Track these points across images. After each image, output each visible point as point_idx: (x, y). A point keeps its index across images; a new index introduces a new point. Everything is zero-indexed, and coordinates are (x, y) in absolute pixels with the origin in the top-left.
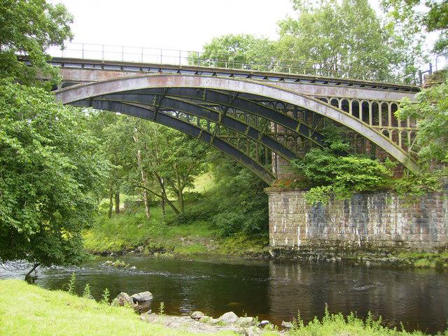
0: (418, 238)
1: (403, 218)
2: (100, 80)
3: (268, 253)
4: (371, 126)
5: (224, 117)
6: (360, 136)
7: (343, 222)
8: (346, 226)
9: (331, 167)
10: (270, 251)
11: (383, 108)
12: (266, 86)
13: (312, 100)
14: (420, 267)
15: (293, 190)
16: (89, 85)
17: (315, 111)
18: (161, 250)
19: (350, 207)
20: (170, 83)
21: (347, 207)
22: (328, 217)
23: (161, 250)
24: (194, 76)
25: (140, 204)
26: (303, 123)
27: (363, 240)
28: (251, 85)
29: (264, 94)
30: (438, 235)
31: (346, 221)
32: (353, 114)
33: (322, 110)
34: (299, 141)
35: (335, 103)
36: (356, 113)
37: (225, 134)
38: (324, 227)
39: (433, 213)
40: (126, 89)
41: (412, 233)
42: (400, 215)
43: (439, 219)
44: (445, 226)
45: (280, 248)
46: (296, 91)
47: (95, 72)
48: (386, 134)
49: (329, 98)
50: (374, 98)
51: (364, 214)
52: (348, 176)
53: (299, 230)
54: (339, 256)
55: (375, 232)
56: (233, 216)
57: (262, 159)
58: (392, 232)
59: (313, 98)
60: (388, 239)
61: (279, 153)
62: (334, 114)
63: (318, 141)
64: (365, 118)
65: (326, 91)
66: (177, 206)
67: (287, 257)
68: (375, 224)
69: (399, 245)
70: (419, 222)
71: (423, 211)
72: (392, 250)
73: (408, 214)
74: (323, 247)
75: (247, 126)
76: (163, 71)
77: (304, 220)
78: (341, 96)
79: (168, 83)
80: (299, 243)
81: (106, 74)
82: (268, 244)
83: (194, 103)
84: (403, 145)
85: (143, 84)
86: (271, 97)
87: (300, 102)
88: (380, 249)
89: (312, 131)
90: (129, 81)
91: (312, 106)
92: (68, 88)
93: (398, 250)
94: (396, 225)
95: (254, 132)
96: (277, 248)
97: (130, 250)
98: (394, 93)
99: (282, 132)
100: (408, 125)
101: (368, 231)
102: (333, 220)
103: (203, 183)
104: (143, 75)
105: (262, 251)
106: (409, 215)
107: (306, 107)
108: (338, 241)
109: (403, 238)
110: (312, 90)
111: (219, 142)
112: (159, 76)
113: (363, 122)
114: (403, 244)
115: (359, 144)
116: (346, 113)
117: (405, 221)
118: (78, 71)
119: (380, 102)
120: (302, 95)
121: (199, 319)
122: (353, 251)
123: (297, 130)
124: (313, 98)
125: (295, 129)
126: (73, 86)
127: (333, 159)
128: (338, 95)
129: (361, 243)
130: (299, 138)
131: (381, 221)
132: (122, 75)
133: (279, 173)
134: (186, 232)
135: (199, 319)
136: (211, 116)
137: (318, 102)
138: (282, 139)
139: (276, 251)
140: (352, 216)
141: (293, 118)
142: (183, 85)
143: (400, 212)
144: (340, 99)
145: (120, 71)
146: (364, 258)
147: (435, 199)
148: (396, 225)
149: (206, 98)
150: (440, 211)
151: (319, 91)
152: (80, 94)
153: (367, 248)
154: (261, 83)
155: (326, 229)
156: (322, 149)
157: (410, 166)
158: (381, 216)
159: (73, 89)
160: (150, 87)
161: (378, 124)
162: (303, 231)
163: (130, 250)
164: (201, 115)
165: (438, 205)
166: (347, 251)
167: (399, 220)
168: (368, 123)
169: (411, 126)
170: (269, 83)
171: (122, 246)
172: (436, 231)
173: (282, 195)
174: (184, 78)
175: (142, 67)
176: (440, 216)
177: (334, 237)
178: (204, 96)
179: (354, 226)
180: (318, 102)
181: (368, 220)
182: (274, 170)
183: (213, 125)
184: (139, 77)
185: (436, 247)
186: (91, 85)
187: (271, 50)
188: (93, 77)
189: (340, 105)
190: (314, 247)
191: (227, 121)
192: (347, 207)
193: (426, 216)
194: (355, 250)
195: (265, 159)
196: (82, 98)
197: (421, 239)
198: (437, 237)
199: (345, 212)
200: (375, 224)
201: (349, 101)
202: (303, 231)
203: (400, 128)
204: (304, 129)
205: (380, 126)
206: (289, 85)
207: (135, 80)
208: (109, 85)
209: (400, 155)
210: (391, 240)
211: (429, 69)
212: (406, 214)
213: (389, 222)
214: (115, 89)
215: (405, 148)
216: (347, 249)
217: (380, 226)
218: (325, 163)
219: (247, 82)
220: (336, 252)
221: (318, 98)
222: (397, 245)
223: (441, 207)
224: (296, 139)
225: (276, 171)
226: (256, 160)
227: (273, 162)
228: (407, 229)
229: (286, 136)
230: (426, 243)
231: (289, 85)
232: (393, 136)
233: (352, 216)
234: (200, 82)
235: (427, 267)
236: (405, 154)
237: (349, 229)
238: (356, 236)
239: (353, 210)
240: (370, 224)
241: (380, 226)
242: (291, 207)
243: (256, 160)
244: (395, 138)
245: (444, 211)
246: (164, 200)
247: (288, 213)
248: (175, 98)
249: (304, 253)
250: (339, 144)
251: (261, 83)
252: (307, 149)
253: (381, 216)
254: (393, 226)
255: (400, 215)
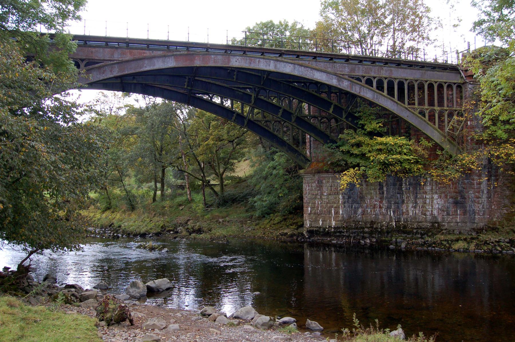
0: (456, 220)
1: (439, 200)
2: (124, 59)
3: (302, 234)
4: (406, 106)
5: (257, 99)
6: (395, 116)
7: (377, 203)
8: (380, 207)
9: (365, 149)
10: (304, 233)
11: (419, 88)
12: (298, 65)
13: (346, 79)
14: (458, 251)
15: (327, 172)
16: (113, 64)
17: (349, 90)
18: (199, 231)
19: (385, 189)
20: (198, 63)
21: (381, 188)
22: (362, 198)
23: (199, 231)
24: (222, 55)
25: (182, 187)
26: (337, 104)
27: (398, 221)
28: (283, 64)
29: (296, 73)
30: (476, 217)
31: (381, 202)
32: (388, 94)
33: (356, 90)
34: (333, 123)
35: (369, 82)
36: (391, 92)
37: (257, 114)
38: (358, 208)
39: (471, 194)
40: (152, 68)
41: (448, 214)
42: (436, 196)
43: (477, 200)
44: (483, 208)
45: (315, 229)
46: (329, 70)
47: (119, 51)
48: (422, 113)
49: (364, 77)
50: (410, 77)
51: (399, 195)
52: (382, 157)
53: (333, 211)
54: (373, 237)
55: (411, 214)
56: (268, 199)
57: (296, 141)
58: (428, 213)
59: (347, 77)
60: (423, 220)
61: (313, 135)
62: (368, 94)
63: (352, 122)
64: (401, 98)
65: (360, 71)
66: (217, 189)
67: (320, 239)
68: (411, 205)
69: (436, 227)
70: (456, 203)
71: (460, 192)
72: (427, 232)
73: (443, 195)
74: (357, 228)
75: (280, 108)
76: (191, 49)
77: (339, 202)
78: (375, 75)
79: (196, 61)
80: (333, 223)
81: (131, 53)
82: (302, 226)
83: (226, 85)
84: (439, 125)
85: (171, 63)
86: (302, 76)
87: (334, 82)
88: (415, 231)
89: (345, 112)
90: (155, 60)
91: (345, 85)
92: (91, 67)
93: (434, 231)
94: (432, 206)
95: (287, 114)
96: (312, 229)
97: (169, 231)
98: (432, 72)
99: (316, 114)
100: (445, 105)
101: (403, 213)
102: (368, 201)
103: (243, 169)
104: (170, 54)
105: (296, 232)
106: (446, 196)
107: (339, 87)
108: (372, 223)
109: (440, 220)
110: (346, 69)
111: (252, 125)
112: (186, 55)
113: (399, 102)
114: (438, 225)
115: (396, 125)
116: (381, 92)
117: (441, 202)
118: (101, 50)
119: (416, 81)
120: (335, 74)
121: (209, 315)
122: (388, 233)
123: (331, 111)
124: (347, 77)
125: (329, 110)
126: (97, 65)
127: (367, 139)
128: (373, 74)
129: (396, 224)
130: (333, 121)
131: (416, 203)
132: (148, 53)
133: (313, 155)
134: (225, 214)
135: (209, 315)
136: (245, 99)
137: (351, 81)
138: (316, 121)
139: (311, 232)
140: (387, 198)
141: (326, 98)
142: (211, 64)
143: (436, 193)
144: (375, 78)
145: (145, 49)
146: (398, 240)
147: (473, 180)
148: (432, 206)
149: (237, 79)
150: (479, 192)
151: (353, 70)
152: (103, 73)
153: (402, 229)
154: (293, 62)
155: (360, 210)
156: (355, 131)
157: (447, 147)
158: (416, 197)
159: (97, 68)
160: (177, 66)
161: (414, 104)
162: (337, 213)
163: (169, 231)
164: (234, 97)
165: (476, 186)
166: (381, 232)
167: (435, 201)
168: (404, 103)
169: (448, 106)
170: (301, 62)
171: (162, 227)
172: (474, 212)
173: (317, 177)
174: (213, 56)
175: (167, 47)
176: (478, 198)
177: (369, 219)
178: (235, 77)
179: (388, 208)
180: (351, 81)
181: (403, 202)
182: (308, 153)
183: (247, 109)
184: (165, 56)
185: (474, 229)
186: (115, 64)
187: (303, 34)
188: (117, 56)
189: (375, 84)
190: (348, 228)
191: (259, 103)
192: (381, 188)
193: (463, 197)
194: (390, 231)
195: (300, 142)
196: (106, 77)
197: (458, 220)
198: (475, 218)
199: (380, 194)
200: (411, 205)
201: (384, 80)
202: (337, 213)
203: (437, 108)
204: (338, 110)
205: (416, 106)
206: (322, 64)
207: (160, 60)
208: (133, 64)
209: (436, 136)
210: (426, 221)
211: (467, 48)
212: (443, 195)
213: (425, 203)
214: (141, 68)
215: (441, 127)
216: (382, 230)
217: (415, 207)
218: (358, 145)
219: (278, 61)
220: (371, 233)
221: (353, 78)
222: (433, 226)
223: (480, 188)
224: (329, 121)
225: (310, 153)
226: (290, 142)
227: (308, 144)
228: (443, 211)
229: (320, 119)
230: (463, 224)
231: (322, 64)
232: (429, 116)
233: (387, 198)
234: (229, 61)
235: (466, 251)
236: (442, 135)
237: (383, 210)
238: (391, 217)
239: (387, 191)
240: (405, 205)
241: (415, 207)
242: (325, 189)
243: (290, 142)
244: (432, 118)
245: (483, 192)
246: (207, 184)
247: (322, 194)
248: (204, 80)
249: (338, 234)
250: (374, 125)
251: (293, 62)
252: (341, 131)
253: (416, 197)
254: (429, 208)
255: (436, 196)
